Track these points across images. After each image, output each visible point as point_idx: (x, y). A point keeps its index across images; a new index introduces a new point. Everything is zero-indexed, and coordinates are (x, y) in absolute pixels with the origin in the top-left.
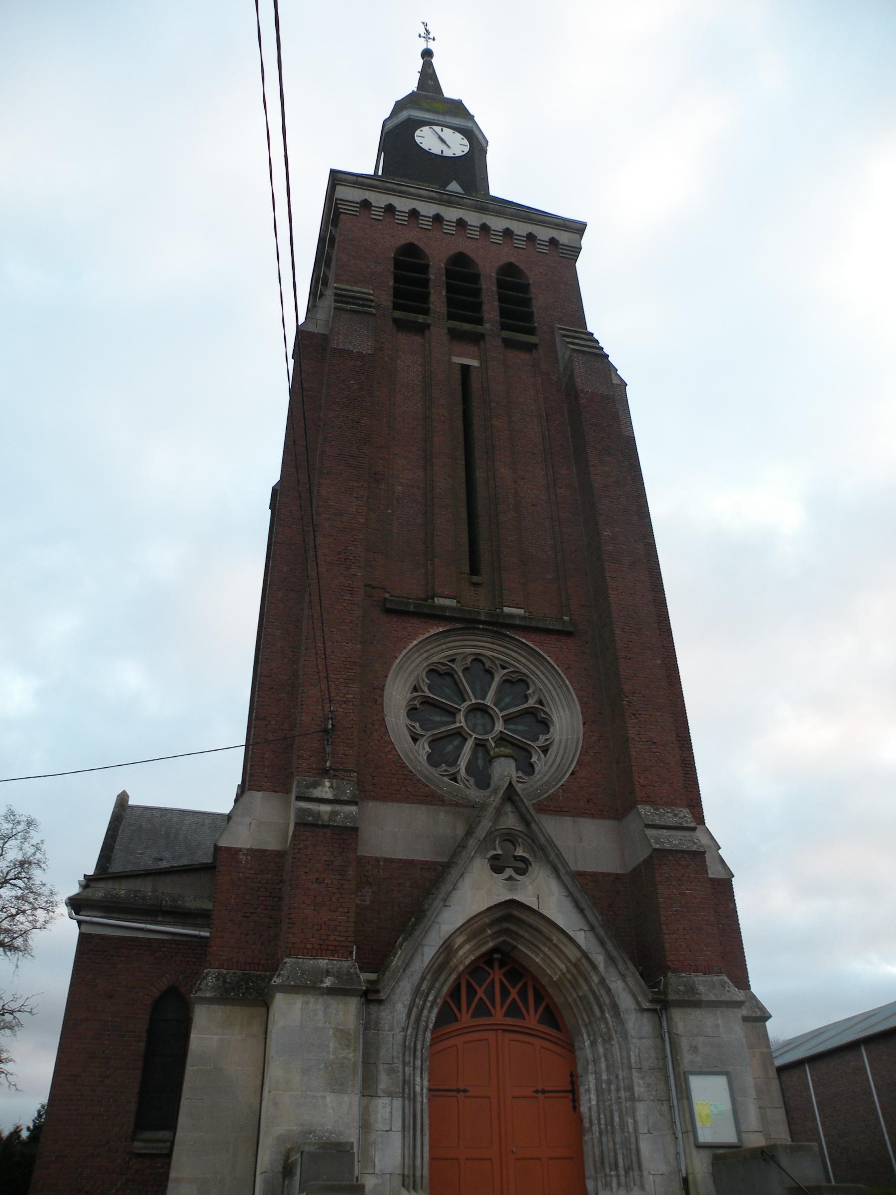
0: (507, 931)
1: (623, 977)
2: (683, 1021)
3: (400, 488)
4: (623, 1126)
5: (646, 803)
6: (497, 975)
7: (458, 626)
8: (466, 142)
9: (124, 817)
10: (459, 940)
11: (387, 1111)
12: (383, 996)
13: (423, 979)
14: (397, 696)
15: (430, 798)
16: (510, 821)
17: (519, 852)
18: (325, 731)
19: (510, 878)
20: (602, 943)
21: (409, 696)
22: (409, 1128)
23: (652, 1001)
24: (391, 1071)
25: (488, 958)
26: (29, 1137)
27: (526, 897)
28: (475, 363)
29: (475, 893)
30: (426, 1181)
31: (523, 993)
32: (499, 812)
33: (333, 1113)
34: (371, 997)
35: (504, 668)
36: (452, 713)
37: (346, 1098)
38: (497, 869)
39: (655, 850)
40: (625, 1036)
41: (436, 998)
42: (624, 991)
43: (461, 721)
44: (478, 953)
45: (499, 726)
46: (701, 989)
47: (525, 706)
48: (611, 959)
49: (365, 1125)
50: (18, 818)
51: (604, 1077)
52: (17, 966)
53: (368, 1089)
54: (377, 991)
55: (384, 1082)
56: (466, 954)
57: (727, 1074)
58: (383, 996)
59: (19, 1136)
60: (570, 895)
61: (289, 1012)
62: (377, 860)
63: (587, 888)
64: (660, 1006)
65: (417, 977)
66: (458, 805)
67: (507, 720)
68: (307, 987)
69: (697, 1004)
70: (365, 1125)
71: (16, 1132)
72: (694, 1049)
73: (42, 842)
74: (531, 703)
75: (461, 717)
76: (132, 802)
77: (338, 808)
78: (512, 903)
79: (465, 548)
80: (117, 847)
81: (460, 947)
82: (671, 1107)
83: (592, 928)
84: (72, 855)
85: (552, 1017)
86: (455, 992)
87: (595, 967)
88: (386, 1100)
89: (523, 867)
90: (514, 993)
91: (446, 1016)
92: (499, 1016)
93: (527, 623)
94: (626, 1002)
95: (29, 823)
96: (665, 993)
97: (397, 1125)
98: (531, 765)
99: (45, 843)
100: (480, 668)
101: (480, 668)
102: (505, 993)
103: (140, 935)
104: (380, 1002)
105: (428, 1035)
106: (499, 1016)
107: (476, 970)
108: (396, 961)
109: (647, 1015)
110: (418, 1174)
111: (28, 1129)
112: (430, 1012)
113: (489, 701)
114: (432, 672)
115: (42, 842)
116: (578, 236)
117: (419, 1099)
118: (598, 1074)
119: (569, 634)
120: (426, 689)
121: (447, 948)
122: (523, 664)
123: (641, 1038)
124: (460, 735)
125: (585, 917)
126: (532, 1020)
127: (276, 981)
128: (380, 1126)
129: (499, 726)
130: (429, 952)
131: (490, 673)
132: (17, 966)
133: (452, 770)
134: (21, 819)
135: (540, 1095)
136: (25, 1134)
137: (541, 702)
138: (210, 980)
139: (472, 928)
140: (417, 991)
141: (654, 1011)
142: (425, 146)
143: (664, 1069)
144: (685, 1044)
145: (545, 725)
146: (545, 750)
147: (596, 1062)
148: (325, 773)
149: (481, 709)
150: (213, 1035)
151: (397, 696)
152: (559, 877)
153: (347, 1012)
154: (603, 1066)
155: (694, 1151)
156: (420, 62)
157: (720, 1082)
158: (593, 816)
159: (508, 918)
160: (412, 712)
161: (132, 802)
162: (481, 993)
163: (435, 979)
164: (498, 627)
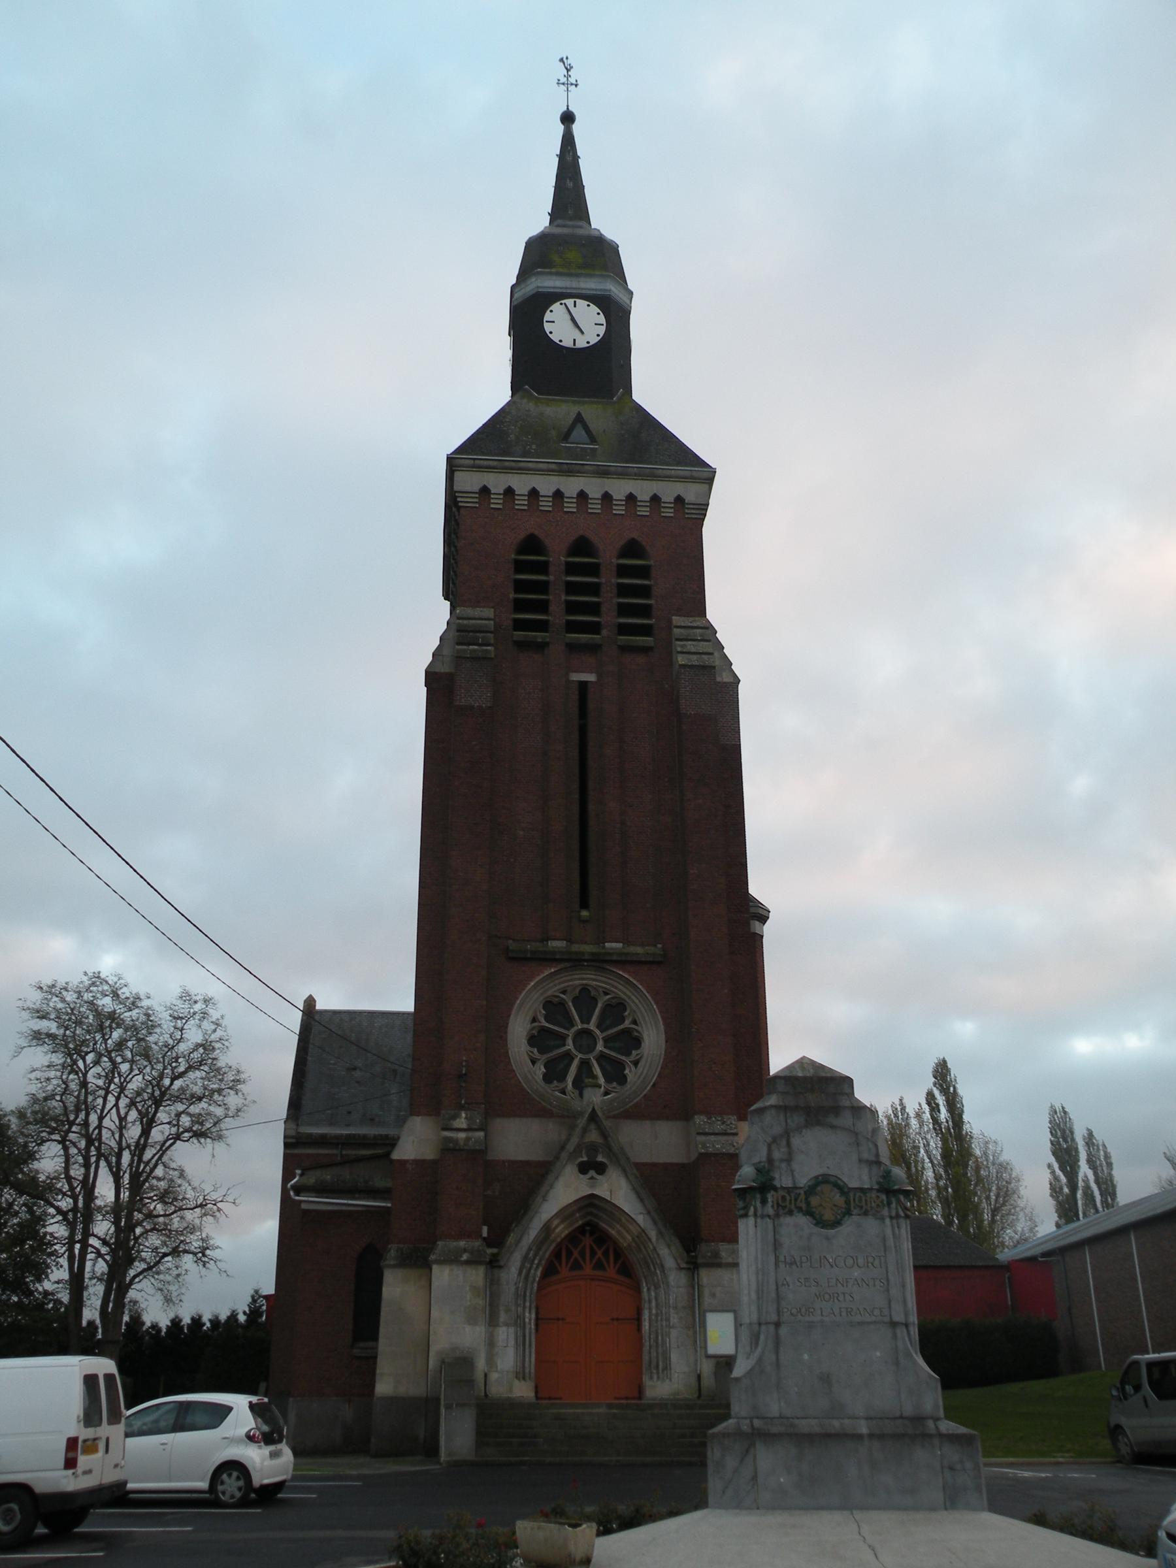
0: (591, 1214)
1: (669, 1246)
2: (706, 1276)
3: (521, 833)
4: (664, 1342)
5: (701, 1113)
6: (587, 1241)
7: (563, 965)
8: (602, 319)
9: (314, 1022)
10: (556, 1222)
11: (505, 1335)
12: (502, 1263)
13: (530, 1249)
14: (518, 1030)
15: (541, 1112)
16: (594, 1136)
17: (600, 1158)
18: (461, 1076)
19: (592, 1178)
20: (655, 1223)
21: (529, 1026)
22: (521, 1343)
23: (687, 1263)
24: (508, 1311)
25: (581, 1230)
26: (246, 1321)
27: (602, 1191)
28: (591, 678)
29: (566, 1190)
30: (533, 1375)
31: (606, 1253)
32: (585, 1130)
33: (470, 1336)
34: (494, 1264)
35: (606, 994)
36: (563, 1038)
37: (478, 1328)
38: (583, 1169)
39: (701, 1154)
40: (667, 1284)
41: (540, 1261)
42: (668, 1255)
43: (570, 1045)
44: (571, 1229)
45: (600, 1047)
46: (723, 1254)
47: (622, 1027)
48: (660, 1234)
49: (491, 1343)
50: (195, 998)
51: (654, 1311)
52: (213, 1156)
53: (493, 1322)
54: (498, 1261)
55: (503, 1317)
56: (561, 1231)
57: (735, 1312)
58: (502, 1263)
59: (237, 1320)
60: (634, 1189)
61: (442, 1276)
62: (504, 1162)
63: (652, 1180)
64: (693, 1266)
65: (525, 1249)
66: (567, 1116)
67: (606, 1041)
68: (452, 1259)
69: (719, 1265)
70: (491, 1343)
71: (233, 1316)
72: (713, 1295)
73: (222, 1017)
74: (627, 1024)
75: (570, 1041)
76: (319, 1006)
77: (470, 1134)
78: (592, 1196)
79: (577, 887)
80: (309, 1058)
81: (557, 1227)
82: (695, 1332)
83: (649, 1213)
84: (268, 1063)
85: (626, 1270)
86: (557, 1254)
87: (650, 1240)
88: (504, 1329)
89: (601, 1169)
90: (599, 1253)
91: (550, 1271)
92: (588, 1270)
93: (623, 958)
94: (670, 1262)
95: (207, 1001)
96: (696, 1257)
97: (512, 1342)
98: (625, 1077)
99: (226, 1018)
100: (585, 999)
101: (585, 999)
102: (593, 1253)
103: (344, 1208)
104: (500, 1267)
105: (536, 1285)
106: (588, 1270)
107: (573, 1238)
108: (511, 1239)
109: (684, 1272)
110: (527, 1371)
111: (245, 1313)
112: (536, 1269)
113: (592, 1026)
114: (548, 1004)
115: (222, 1017)
116: (706, 486)
117: (528, 1326)
118: (650, 1309)
119: (659, 963)
120: (542, 1020)
121: (547, 1228)
122: (621, 991)
123: (679, 1287)
124: (569, 1057)
125: (644, 1205)
126: (611, 1271)
127: (432, 1257)
128: (500, 1344)
129: (600, 1047)
130: (534, 1230)
131: (595, 1000)
132: (213, 1156)
133: (562, 1086)
134: (197, 998)
135: (615, 1323)
136: (242, 1318)
137: (635, 1022)
138: (393, 1253)
139: (564, 1214)
140: (525, 1258)
141: (689, 1269)
142: (555, 338)
143: (694, 1306)
144: (706, 1292)
145: (637, 1042)
146: (636, 1063)
147: (650, 1301)
148: (462, 1108)
149: (587, 1033)
150: (396, 1287)
151: (518, 1030)
152: (627, 1176)
153: (477, 1275)
154: (654, 1304)
155: (704, 1360)
156: (561, 128)
157: (729, 1317)
158: (667, 1118)
159: (591, 1205)
160: (532, 1040)
161: (319, 1006)
162: (576, 1254)
163: (539, 1249)
164: (600, 962)
